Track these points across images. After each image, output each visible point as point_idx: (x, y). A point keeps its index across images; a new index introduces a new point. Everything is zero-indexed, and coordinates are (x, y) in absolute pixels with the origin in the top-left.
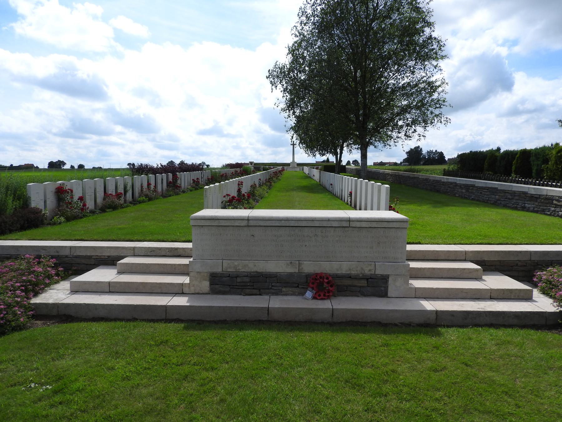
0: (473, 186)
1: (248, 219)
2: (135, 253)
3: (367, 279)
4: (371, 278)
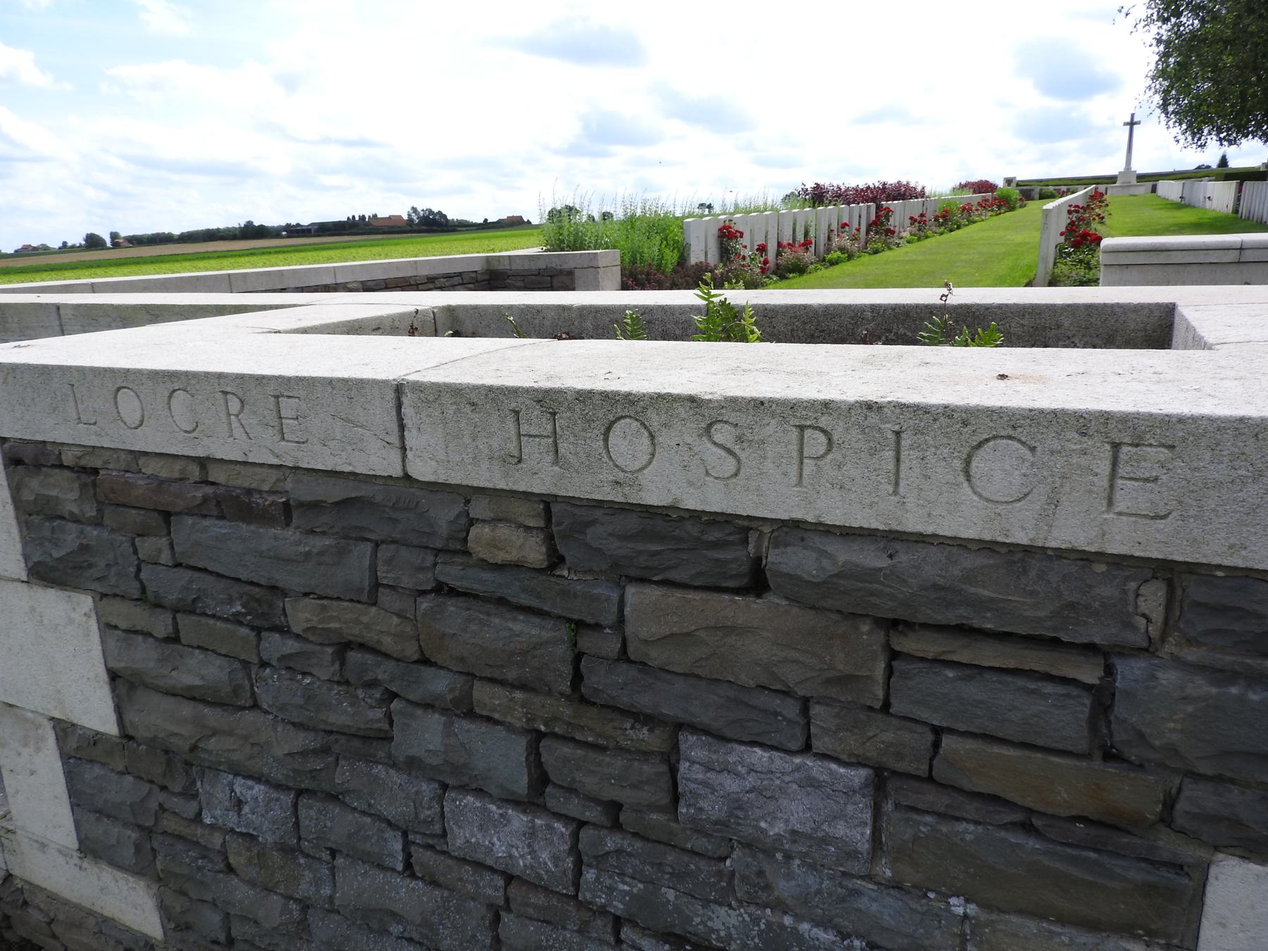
4: (362, 647)
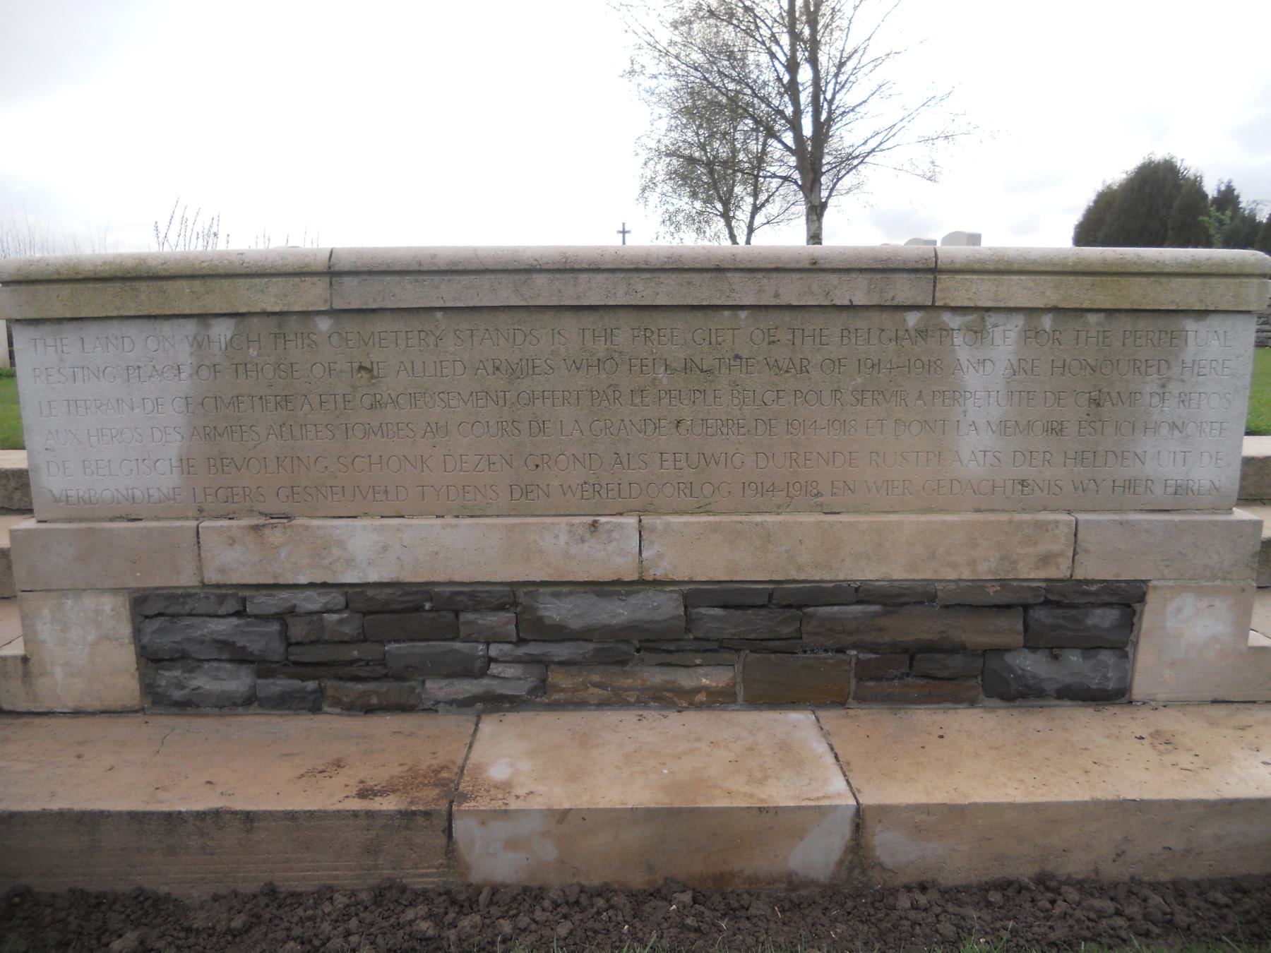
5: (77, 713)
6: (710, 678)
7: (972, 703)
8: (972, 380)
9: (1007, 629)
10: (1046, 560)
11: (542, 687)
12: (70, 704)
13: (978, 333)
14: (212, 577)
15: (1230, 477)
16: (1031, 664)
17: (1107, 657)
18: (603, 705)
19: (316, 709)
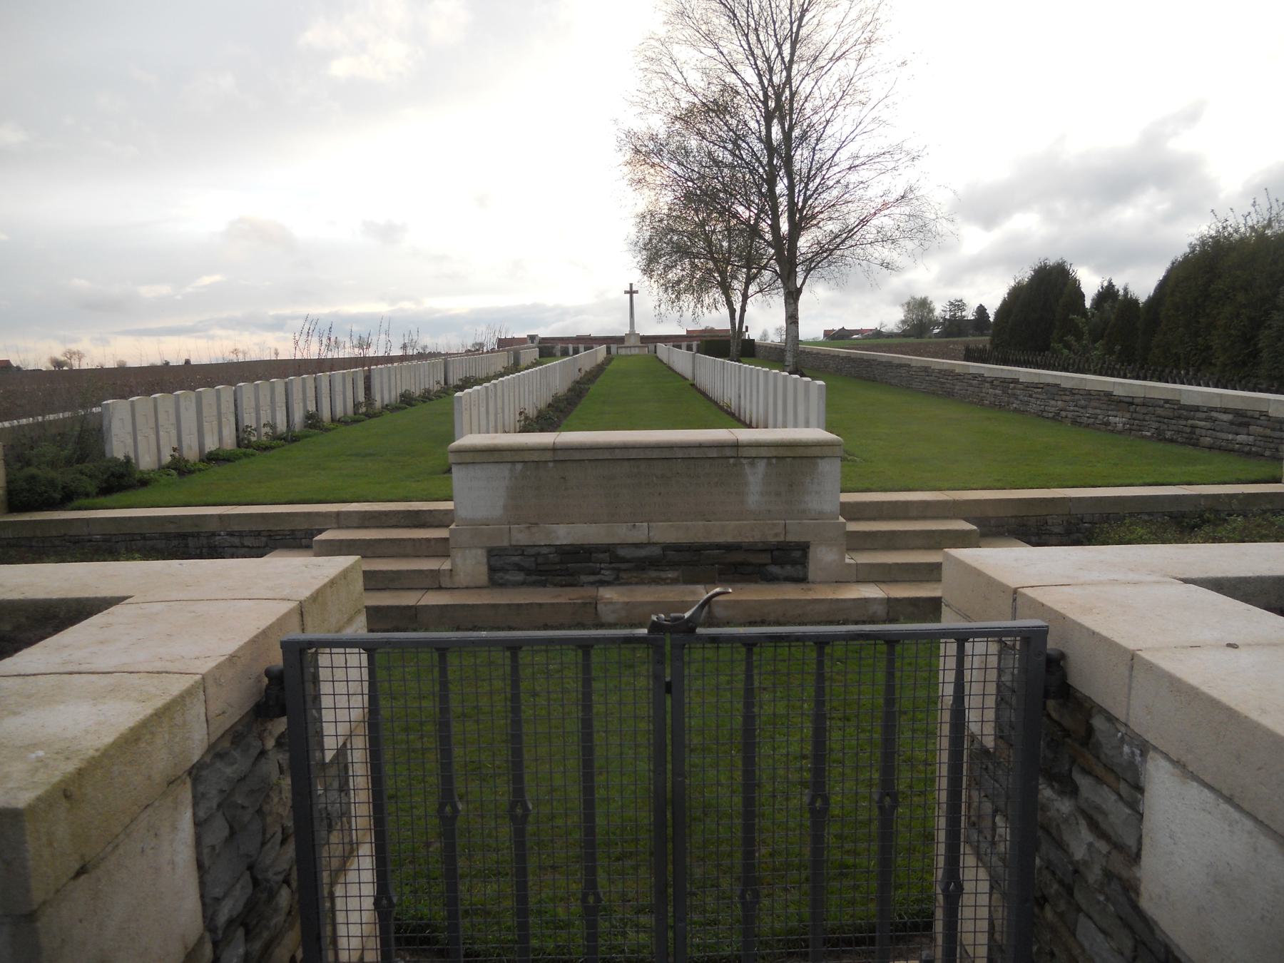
0: (1016, 381)
1: (554, 449)
2: (340, 520)
3: (772, 551)
5: (467, 588)
6: (670, 575)
7: (756, 582)
8: (751, 479)
9: (765, 558)
10: (776, 535)
11: (617, 578)
12: (465, 585)
13: (752, 464)
14: (514, 543)
15: (837, 508)
16: (775, 570)
17: (799, 567)
18: (637, 584)
19: (545, 586)
